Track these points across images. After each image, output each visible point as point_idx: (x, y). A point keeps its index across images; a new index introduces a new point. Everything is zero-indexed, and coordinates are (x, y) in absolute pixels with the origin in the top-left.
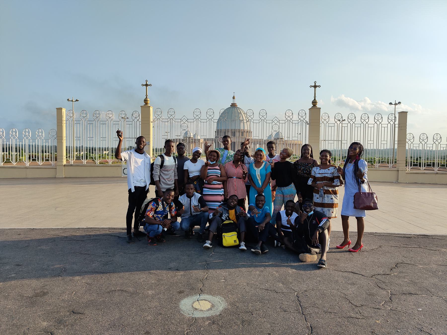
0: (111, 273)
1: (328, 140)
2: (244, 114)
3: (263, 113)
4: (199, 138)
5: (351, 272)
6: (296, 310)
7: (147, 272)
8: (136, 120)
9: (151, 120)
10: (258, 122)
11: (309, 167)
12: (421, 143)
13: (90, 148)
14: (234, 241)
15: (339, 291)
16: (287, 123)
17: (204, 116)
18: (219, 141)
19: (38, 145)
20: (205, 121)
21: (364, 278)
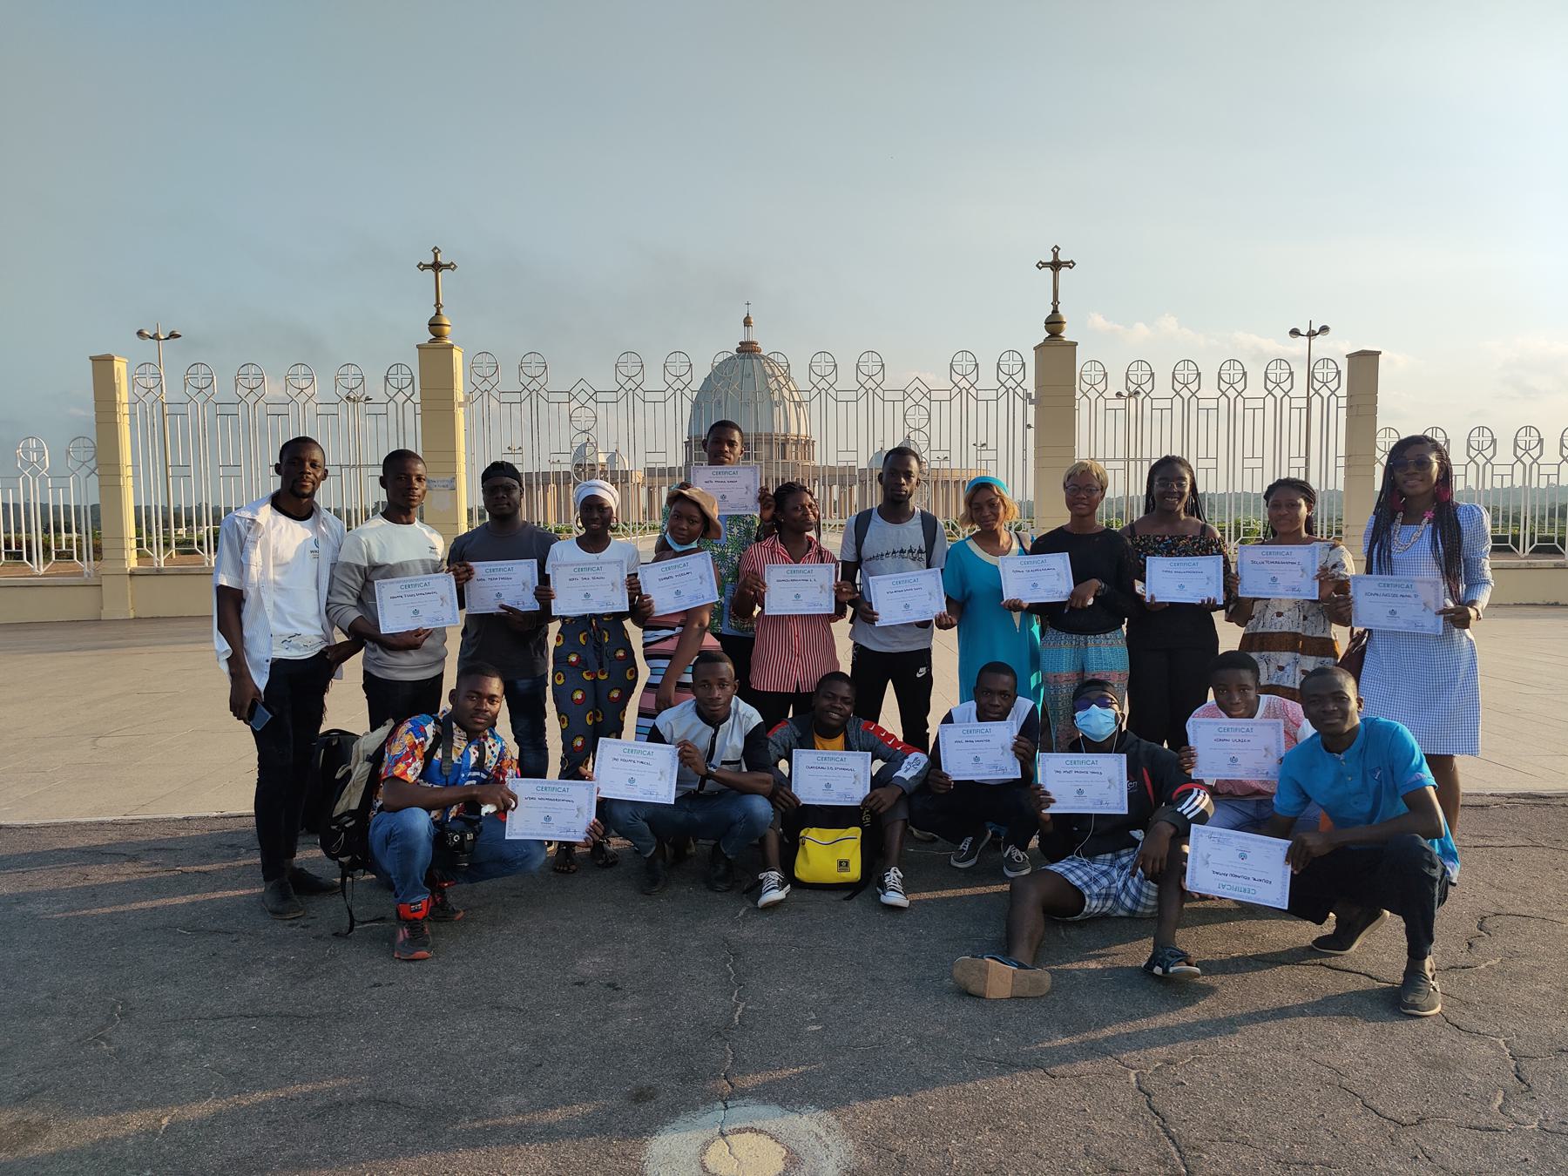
3: (870, 364)
6: (1158, 1161)
8: (401, 398)
9: (459, 395)
10: (852, 396)
12: (1472, 460)
14: (840, 863)
15: (1303, 1056)
17: (847, 379)
20: (660, 397)
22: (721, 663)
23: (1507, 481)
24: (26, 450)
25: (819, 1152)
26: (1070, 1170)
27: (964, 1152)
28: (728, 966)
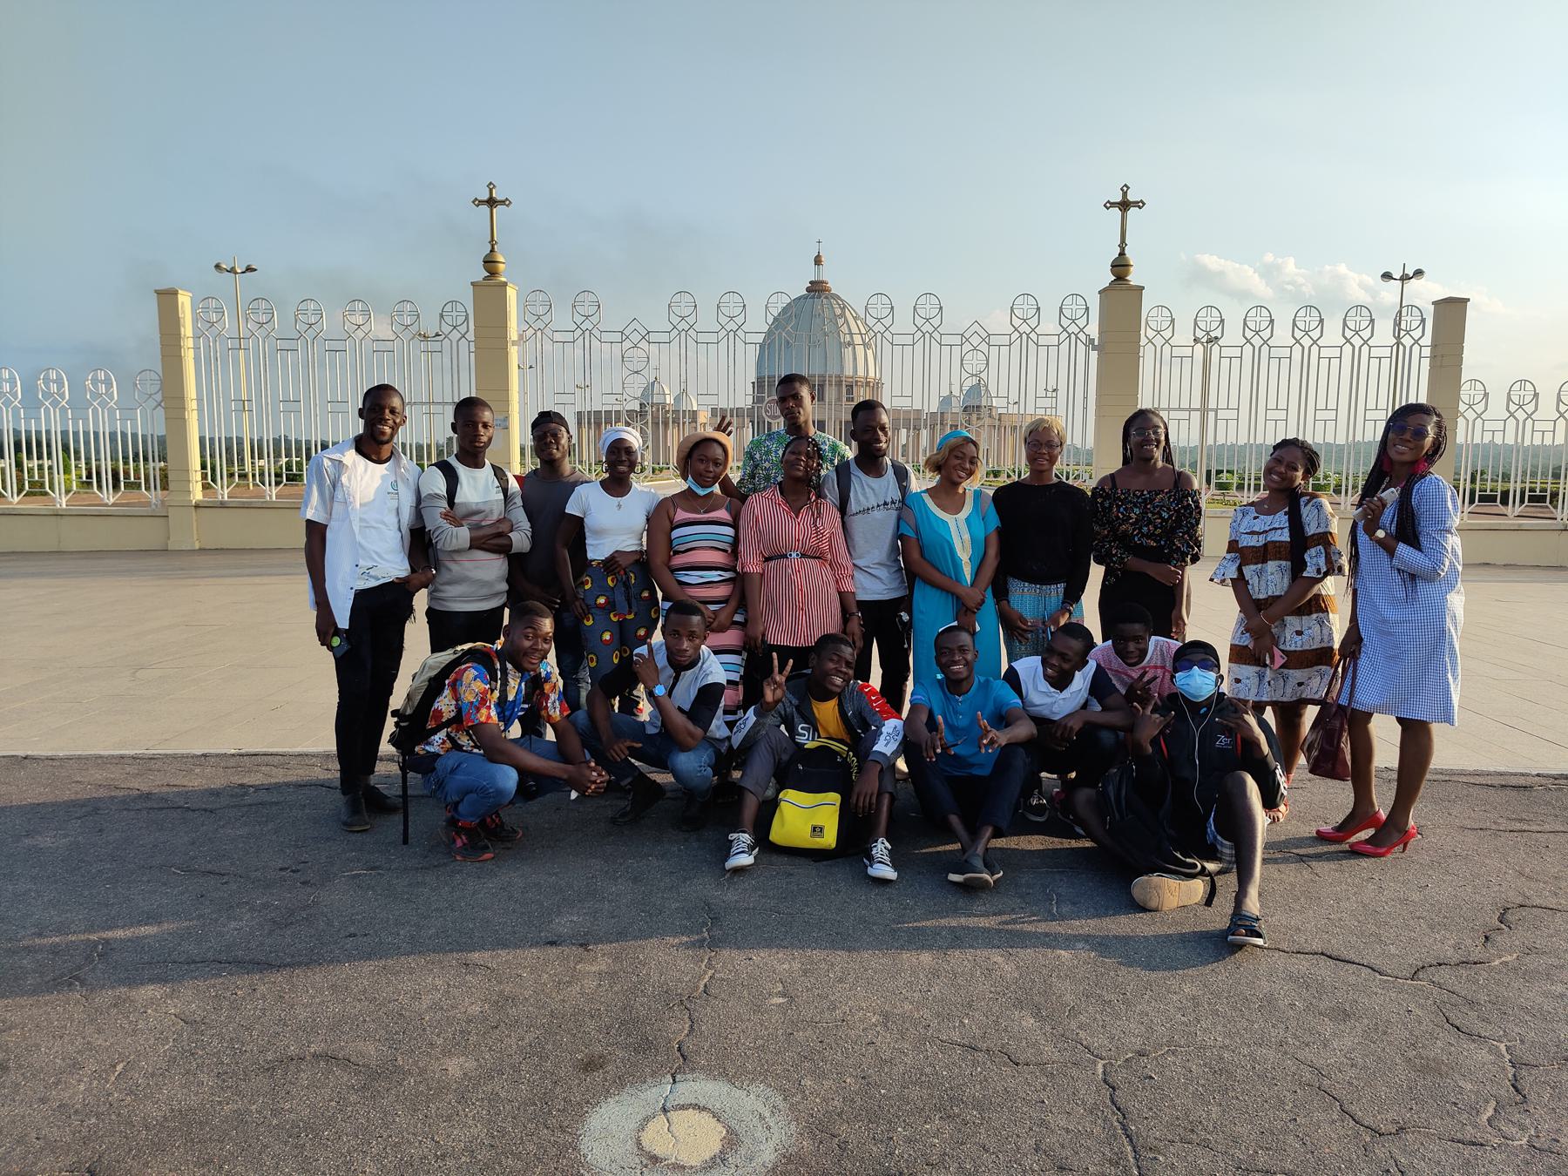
0: (299, 964)
1: (1169, 409)
2: (855, 319)
4: (695, 409)
5: (1322, 954)
6: (1110, 1161)
7: (453, 958)
8: (455, 335)
9: (513, 334)
10: (909, 339)
11: (1157, 506)
13: (308, 442)
14: (814, 829)
15: (1286, 1053)
16: (1016, 347)
17: (707, 320)
18: (764, 414)
19: (86, 430)
21: (1386, 981)
22: (539, 619)
23: (1548, 436)
24: (95, 381)
25: (760, 1133)
26: (1015, 1166)
27: (909, 1141)
28: (704, 930)
